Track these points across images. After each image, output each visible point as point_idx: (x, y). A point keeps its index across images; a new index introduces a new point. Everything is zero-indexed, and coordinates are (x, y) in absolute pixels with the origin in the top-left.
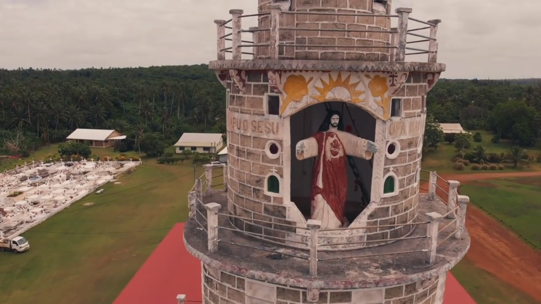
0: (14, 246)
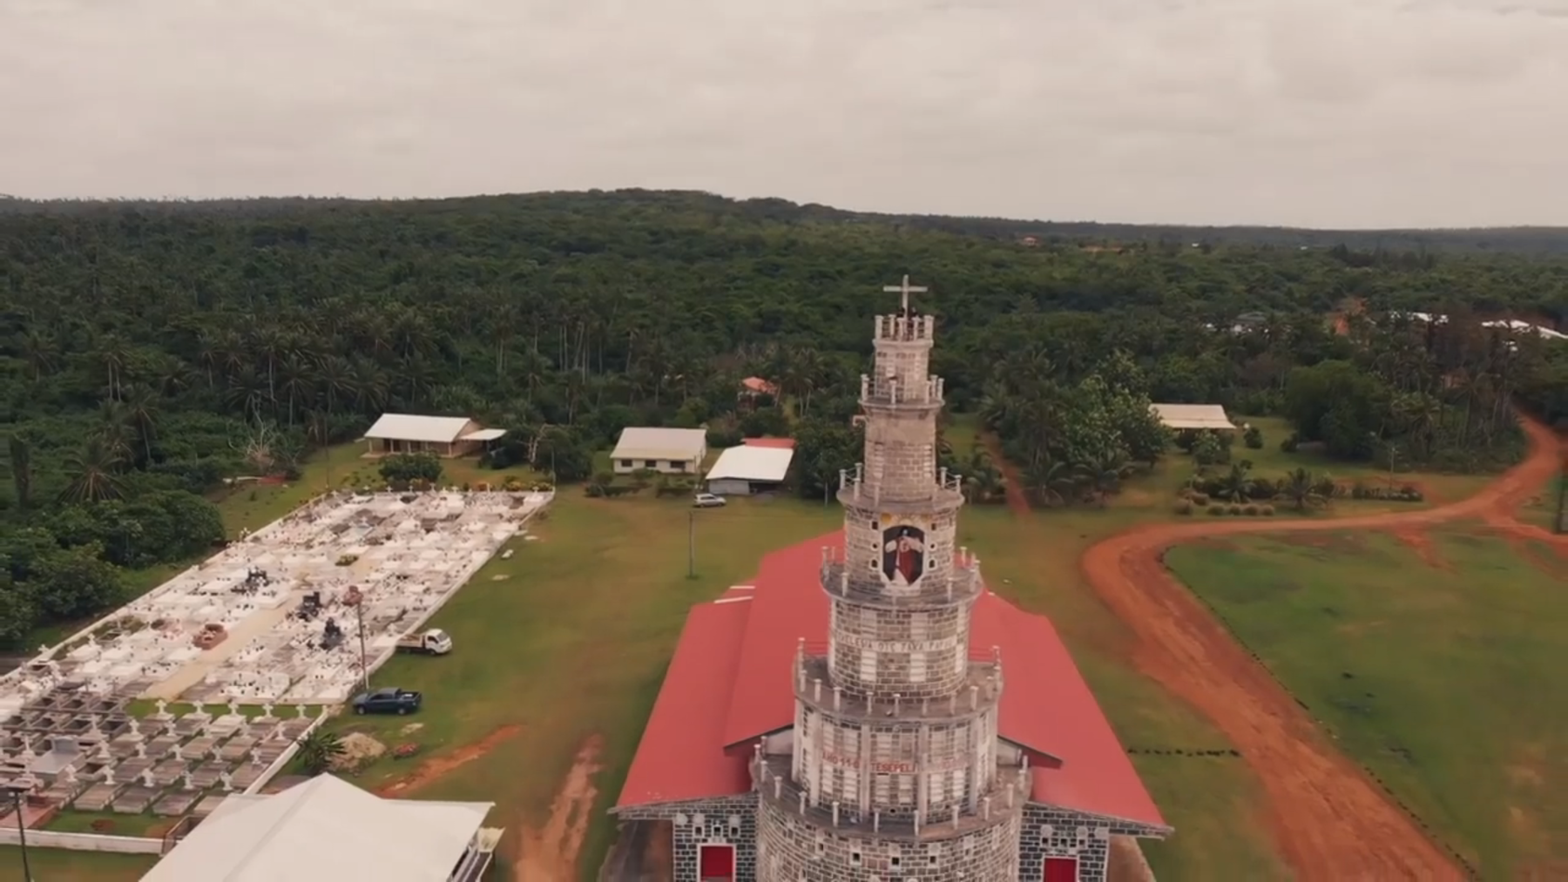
0: (430, 645)
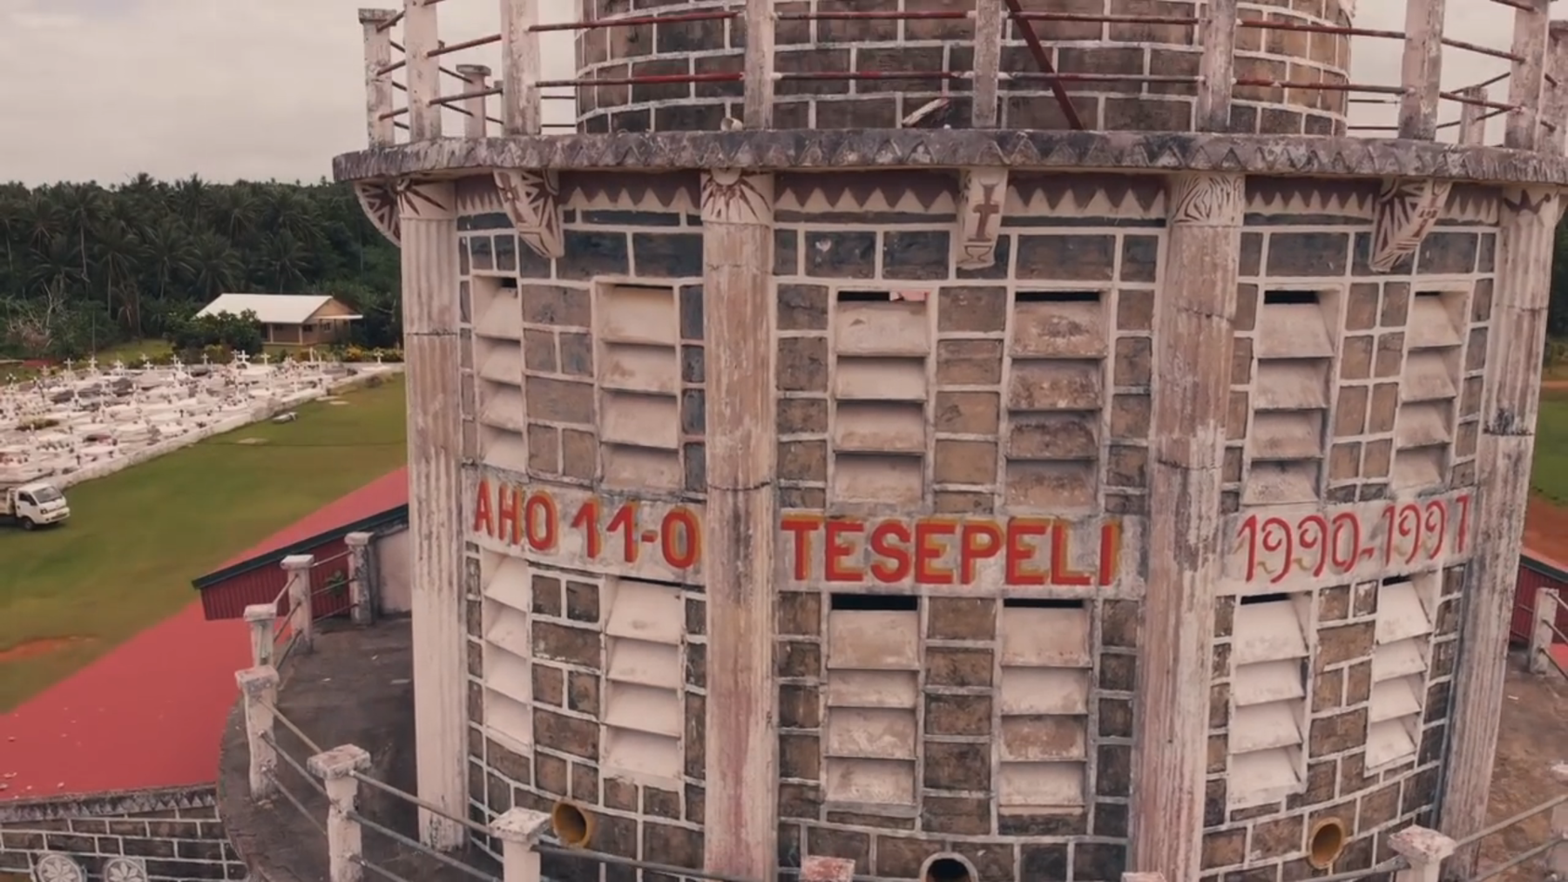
0: (24, 509)
